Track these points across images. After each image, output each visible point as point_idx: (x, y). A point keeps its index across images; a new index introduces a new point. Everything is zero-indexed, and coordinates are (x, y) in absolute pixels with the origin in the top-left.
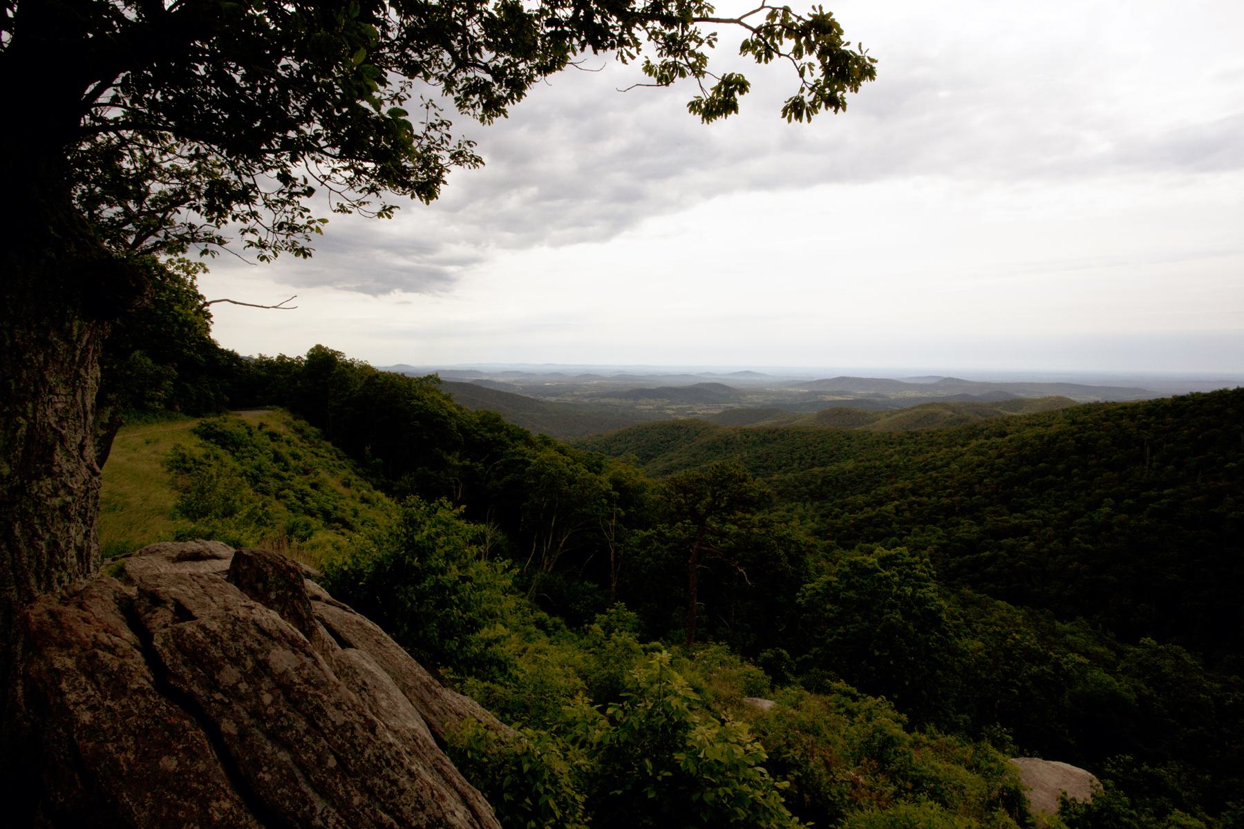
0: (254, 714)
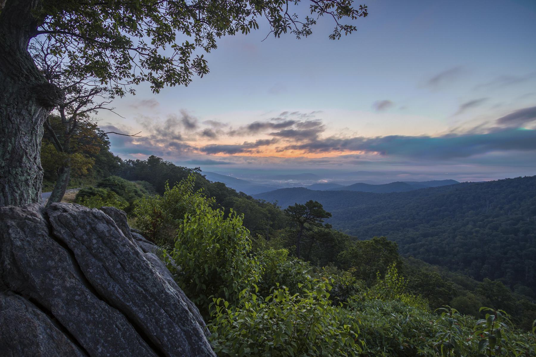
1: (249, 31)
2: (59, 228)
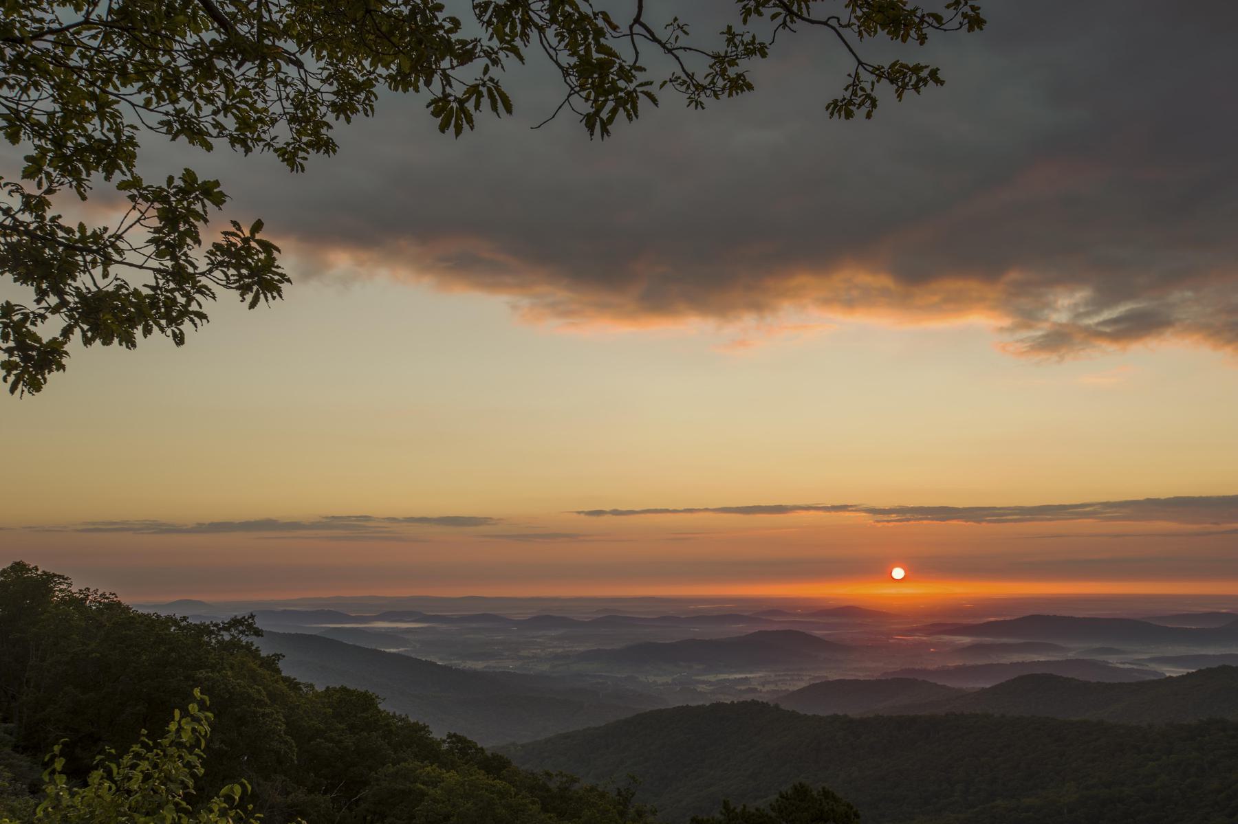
1: (470, 120)
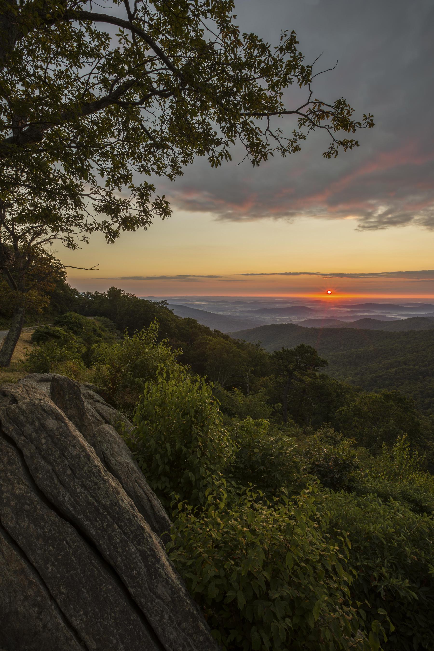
0: (37, 448)
1: (220, 163)
2: (8, 425)
